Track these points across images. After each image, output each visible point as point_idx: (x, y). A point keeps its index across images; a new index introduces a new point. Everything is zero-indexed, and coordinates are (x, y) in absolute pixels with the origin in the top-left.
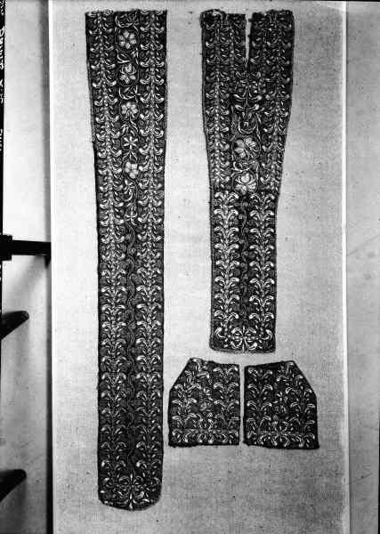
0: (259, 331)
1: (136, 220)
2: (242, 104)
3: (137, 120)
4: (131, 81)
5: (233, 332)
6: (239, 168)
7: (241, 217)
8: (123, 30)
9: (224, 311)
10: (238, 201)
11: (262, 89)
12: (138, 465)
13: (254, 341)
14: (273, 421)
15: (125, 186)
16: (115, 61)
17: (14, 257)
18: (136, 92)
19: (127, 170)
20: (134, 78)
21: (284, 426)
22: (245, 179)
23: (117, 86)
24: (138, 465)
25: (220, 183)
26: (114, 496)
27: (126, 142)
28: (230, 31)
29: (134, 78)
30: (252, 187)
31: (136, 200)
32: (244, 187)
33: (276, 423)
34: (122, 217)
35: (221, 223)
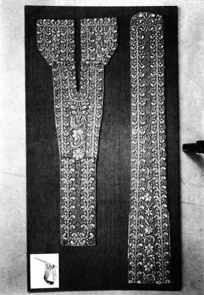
0: (86, 234)
1: (146, 170)
2: (75, 110)
3: (145, 225)
4: (147, 245)
5: (72, 235)
6: (74, 145)
7: (76, 172)
8: (151, 272)
9: (66, 224)
10: (75, 163)
11: (86, 102)
12: (143, 37)
13: (83, 240)
14: (60, 33)
15: (152, 189)
16: (156, 256)
17: (196, 143)
18: (145, 239)
19: (151, 197)
20: (146, 247)
21: (54, 30)
22: (78, 151)
23: (155, 242)
24: (143, 37)
25: (64, 154)
26: (156, 20)
27: (152, 212)
28: (66, 72)
29: (146, 247)
30: (81, 156)
31: (146, 181)
32: (78, 156)
33: (58, 32)
34: (153, 172)
35: (65, 176)
